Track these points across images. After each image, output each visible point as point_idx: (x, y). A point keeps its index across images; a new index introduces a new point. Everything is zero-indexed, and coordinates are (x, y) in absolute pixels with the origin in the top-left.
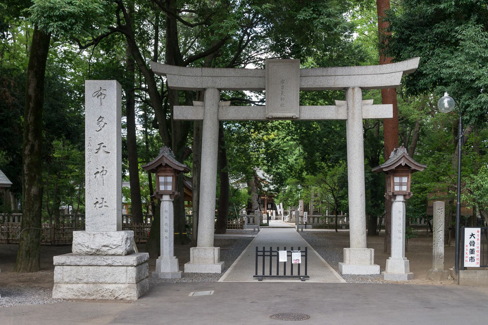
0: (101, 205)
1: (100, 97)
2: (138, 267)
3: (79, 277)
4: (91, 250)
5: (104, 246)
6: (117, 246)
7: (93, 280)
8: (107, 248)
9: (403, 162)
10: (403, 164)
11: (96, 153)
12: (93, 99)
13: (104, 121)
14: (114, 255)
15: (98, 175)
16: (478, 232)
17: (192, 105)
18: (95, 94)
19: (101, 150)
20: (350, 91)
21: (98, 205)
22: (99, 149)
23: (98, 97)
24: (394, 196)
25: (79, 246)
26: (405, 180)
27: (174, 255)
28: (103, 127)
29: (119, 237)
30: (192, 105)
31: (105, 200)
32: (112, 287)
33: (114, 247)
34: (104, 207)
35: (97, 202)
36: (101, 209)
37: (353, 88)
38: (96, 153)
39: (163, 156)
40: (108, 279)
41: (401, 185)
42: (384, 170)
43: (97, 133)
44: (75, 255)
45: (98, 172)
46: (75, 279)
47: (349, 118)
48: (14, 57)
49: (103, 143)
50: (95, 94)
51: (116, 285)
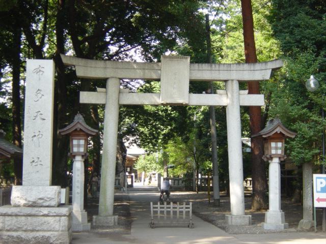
0: (36, 164)
1: (38, 73)
3: (19, 226)
6: (51, 199)
7: (31, 228)
8: (42, 201)
9: (278, 130)
10: (279, 132)
11: (34, 119)
15: (35, 138)
19: (38, 118)
20: (229, 83)
21: (34, 164)
22: (36, 116)
24: (271, 158)
26: (280, 144)
27: (84, 209)
28: (40, 98)
29: (52, 191)
31: (40, 159)
32: (47, 234)
33: (48, 200)
35: (33, 161)
36: (36, 167)
37: (232, 80)
38: (34, 119)
39: (78, 122)
42: (264, 136)
45: (35, 136)
47: (108, 103)
48: (206, 109)
49: (39, 111)
51: (51, 233)
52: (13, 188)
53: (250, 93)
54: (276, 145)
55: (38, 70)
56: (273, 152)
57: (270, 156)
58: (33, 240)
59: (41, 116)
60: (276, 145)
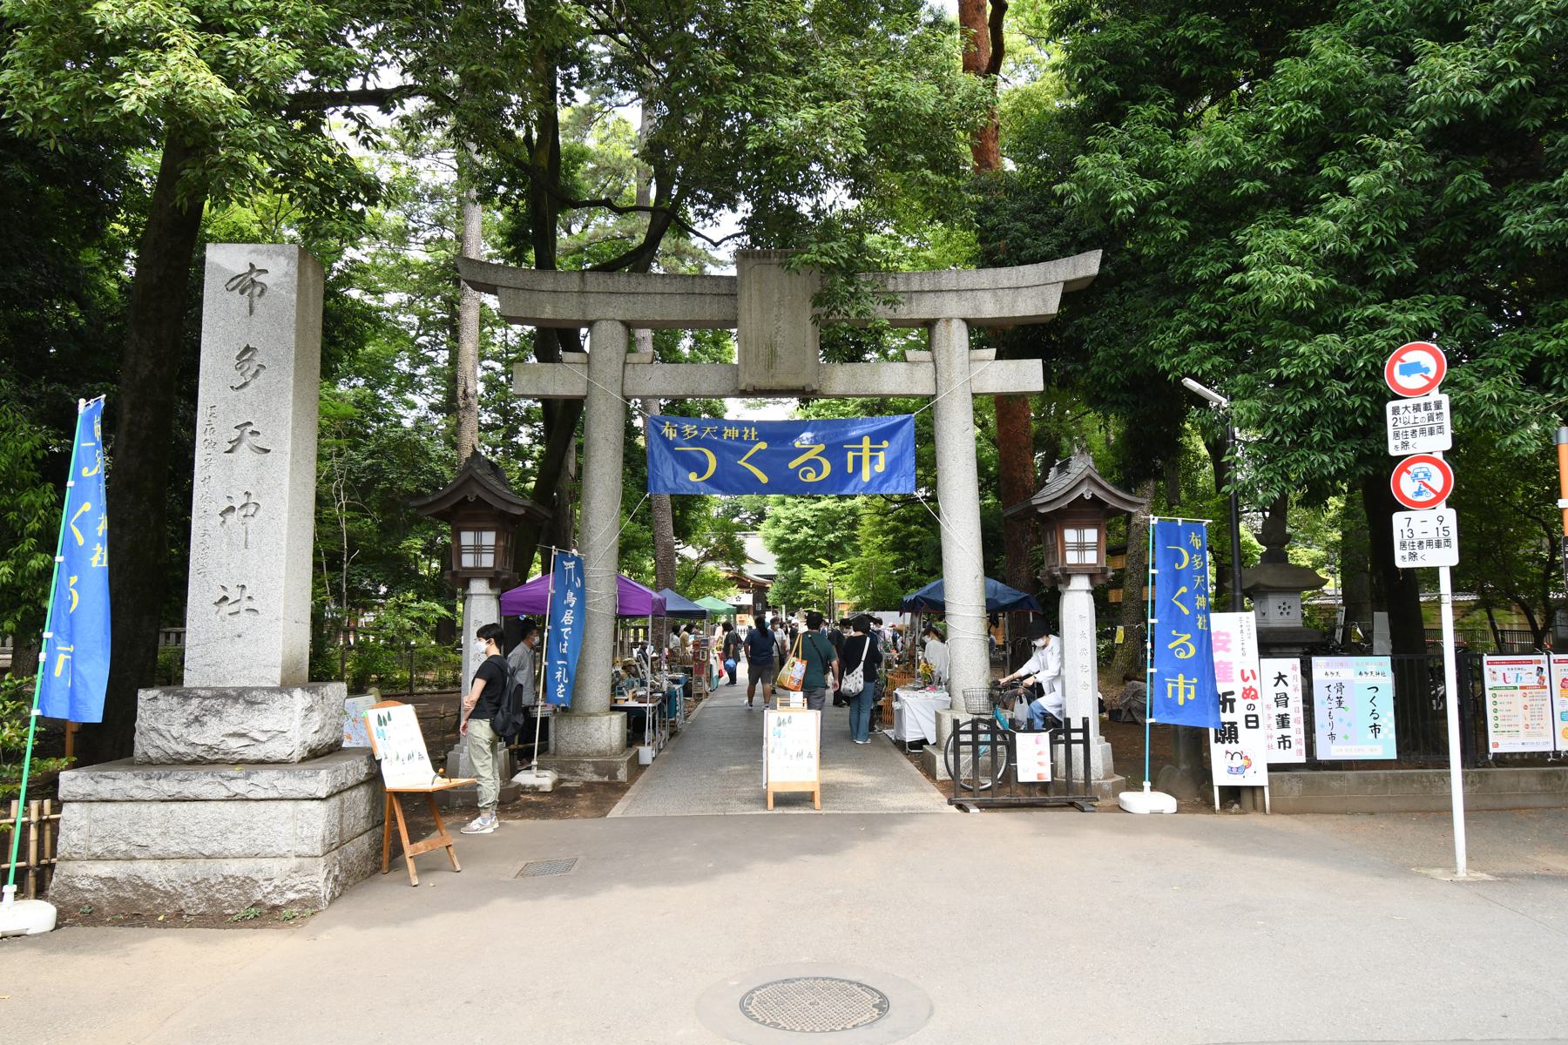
0: (234, 608)
2: (335, 801)
3: (140, 840)
4: (189, 750)
5: (234, 735)
8: (245, 742)
9: (1086, 491)
10: (1088, 497)
12: (228, 295)
13: (258, 360)
14: (261, 762)
15: (231, 518)
16: (1294, 668)
17: (560, 361)
18: (235, 283)
20: (940, 329)
21: (226, 608)
22: (239, 440)
23: (242, 292)
24: (1067, 577)
25: (153, 735)
26: (1091, 535)
30: (560, 361)
31: (247, 593)
33: (263, 738)
34: (244, 614)
35: (225, 599)
36: (235, 618)
37: (949, 320)
40: (234, 844)
41: (1081, 546)
42: (1043, 511)
43: (235, 393)
44: (149, 763)
45: (231, 509)
46: (123, 847)
49: (249, 424)
50: (235, 283)
52: (1501, 749)
53: (999, 357)
54: (478, 539)
55: (247, 282)
56: (1072, 558)
57: (1064, 570)
58: (190, 890)
59: (253, 439)
60: (478, 539)
